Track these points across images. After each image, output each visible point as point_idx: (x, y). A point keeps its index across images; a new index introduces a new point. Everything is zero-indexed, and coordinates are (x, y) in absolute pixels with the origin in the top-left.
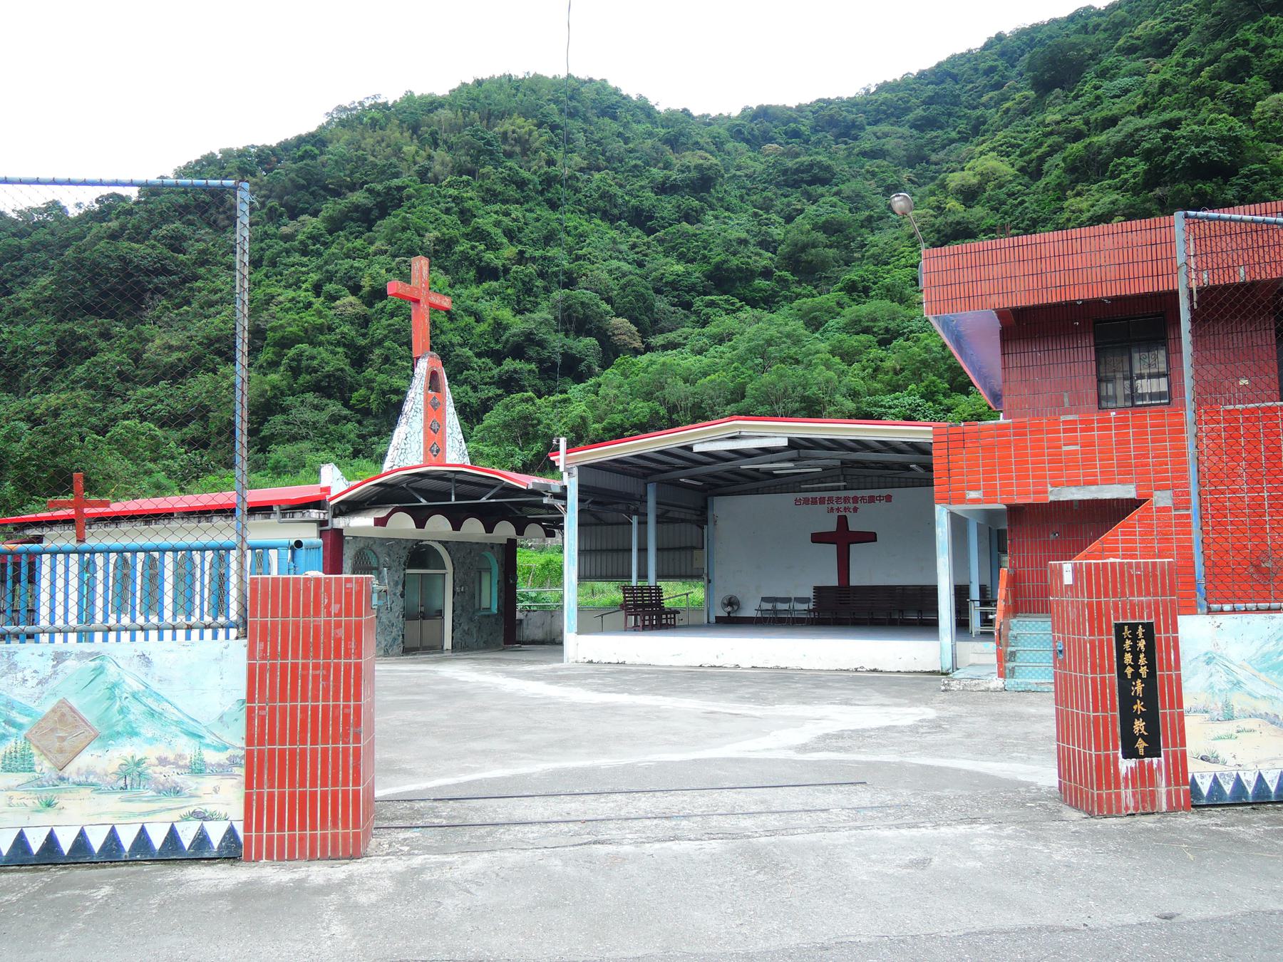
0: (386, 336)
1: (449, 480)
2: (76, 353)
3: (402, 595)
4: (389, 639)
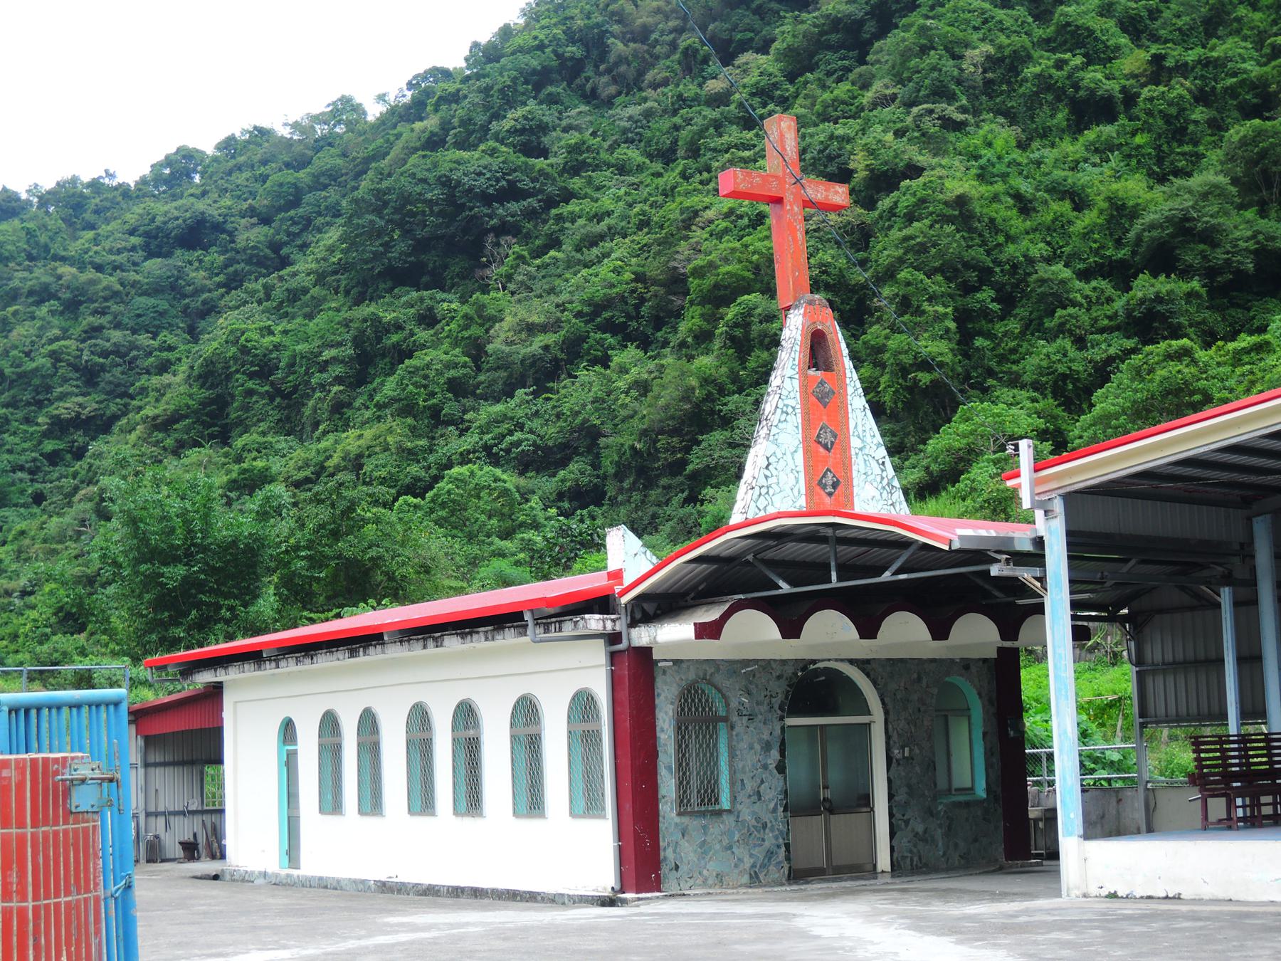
0: (901, 260)
1: (824, 540)
2: (383, 356)
3: (781, 768)
4: (759, 853)
